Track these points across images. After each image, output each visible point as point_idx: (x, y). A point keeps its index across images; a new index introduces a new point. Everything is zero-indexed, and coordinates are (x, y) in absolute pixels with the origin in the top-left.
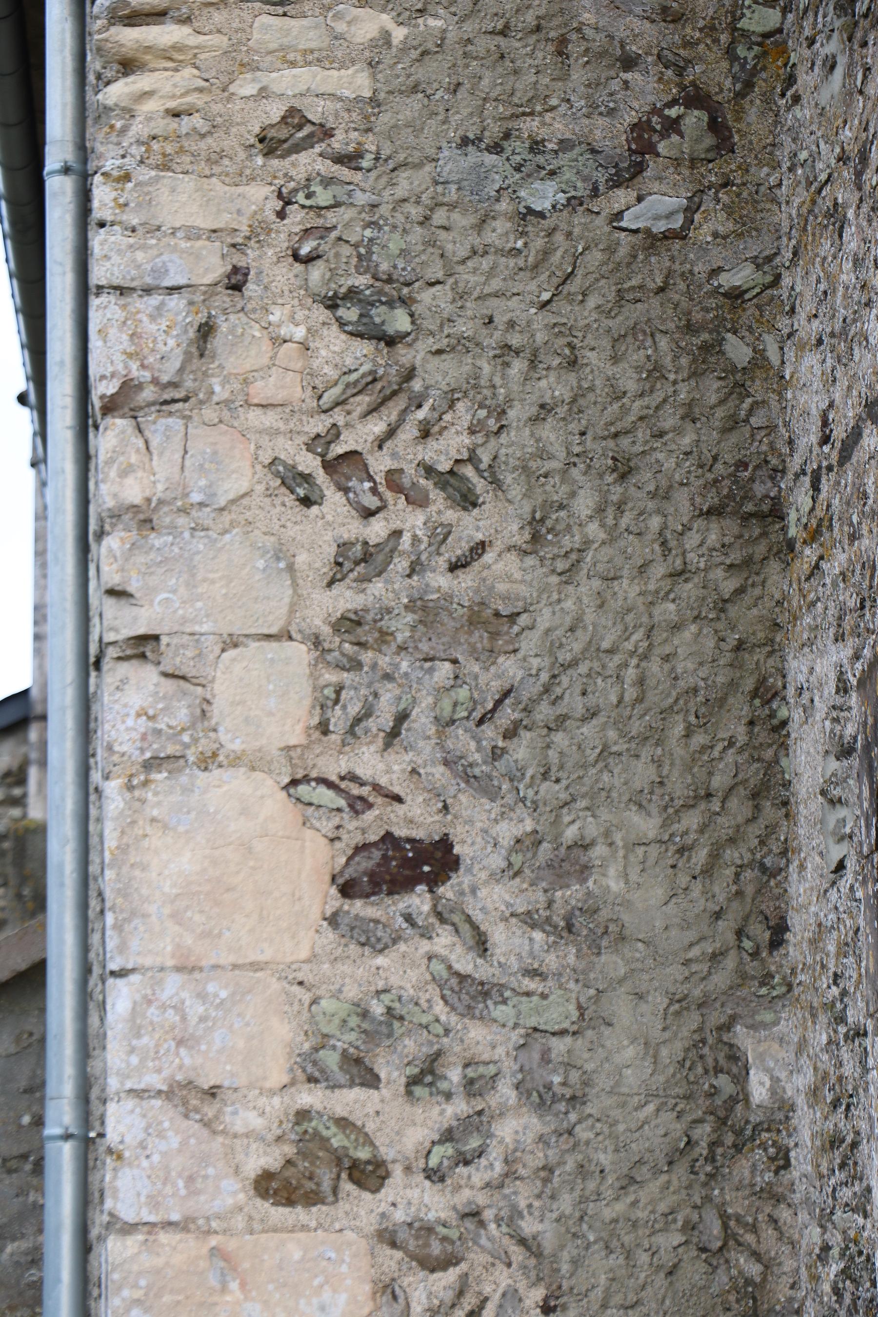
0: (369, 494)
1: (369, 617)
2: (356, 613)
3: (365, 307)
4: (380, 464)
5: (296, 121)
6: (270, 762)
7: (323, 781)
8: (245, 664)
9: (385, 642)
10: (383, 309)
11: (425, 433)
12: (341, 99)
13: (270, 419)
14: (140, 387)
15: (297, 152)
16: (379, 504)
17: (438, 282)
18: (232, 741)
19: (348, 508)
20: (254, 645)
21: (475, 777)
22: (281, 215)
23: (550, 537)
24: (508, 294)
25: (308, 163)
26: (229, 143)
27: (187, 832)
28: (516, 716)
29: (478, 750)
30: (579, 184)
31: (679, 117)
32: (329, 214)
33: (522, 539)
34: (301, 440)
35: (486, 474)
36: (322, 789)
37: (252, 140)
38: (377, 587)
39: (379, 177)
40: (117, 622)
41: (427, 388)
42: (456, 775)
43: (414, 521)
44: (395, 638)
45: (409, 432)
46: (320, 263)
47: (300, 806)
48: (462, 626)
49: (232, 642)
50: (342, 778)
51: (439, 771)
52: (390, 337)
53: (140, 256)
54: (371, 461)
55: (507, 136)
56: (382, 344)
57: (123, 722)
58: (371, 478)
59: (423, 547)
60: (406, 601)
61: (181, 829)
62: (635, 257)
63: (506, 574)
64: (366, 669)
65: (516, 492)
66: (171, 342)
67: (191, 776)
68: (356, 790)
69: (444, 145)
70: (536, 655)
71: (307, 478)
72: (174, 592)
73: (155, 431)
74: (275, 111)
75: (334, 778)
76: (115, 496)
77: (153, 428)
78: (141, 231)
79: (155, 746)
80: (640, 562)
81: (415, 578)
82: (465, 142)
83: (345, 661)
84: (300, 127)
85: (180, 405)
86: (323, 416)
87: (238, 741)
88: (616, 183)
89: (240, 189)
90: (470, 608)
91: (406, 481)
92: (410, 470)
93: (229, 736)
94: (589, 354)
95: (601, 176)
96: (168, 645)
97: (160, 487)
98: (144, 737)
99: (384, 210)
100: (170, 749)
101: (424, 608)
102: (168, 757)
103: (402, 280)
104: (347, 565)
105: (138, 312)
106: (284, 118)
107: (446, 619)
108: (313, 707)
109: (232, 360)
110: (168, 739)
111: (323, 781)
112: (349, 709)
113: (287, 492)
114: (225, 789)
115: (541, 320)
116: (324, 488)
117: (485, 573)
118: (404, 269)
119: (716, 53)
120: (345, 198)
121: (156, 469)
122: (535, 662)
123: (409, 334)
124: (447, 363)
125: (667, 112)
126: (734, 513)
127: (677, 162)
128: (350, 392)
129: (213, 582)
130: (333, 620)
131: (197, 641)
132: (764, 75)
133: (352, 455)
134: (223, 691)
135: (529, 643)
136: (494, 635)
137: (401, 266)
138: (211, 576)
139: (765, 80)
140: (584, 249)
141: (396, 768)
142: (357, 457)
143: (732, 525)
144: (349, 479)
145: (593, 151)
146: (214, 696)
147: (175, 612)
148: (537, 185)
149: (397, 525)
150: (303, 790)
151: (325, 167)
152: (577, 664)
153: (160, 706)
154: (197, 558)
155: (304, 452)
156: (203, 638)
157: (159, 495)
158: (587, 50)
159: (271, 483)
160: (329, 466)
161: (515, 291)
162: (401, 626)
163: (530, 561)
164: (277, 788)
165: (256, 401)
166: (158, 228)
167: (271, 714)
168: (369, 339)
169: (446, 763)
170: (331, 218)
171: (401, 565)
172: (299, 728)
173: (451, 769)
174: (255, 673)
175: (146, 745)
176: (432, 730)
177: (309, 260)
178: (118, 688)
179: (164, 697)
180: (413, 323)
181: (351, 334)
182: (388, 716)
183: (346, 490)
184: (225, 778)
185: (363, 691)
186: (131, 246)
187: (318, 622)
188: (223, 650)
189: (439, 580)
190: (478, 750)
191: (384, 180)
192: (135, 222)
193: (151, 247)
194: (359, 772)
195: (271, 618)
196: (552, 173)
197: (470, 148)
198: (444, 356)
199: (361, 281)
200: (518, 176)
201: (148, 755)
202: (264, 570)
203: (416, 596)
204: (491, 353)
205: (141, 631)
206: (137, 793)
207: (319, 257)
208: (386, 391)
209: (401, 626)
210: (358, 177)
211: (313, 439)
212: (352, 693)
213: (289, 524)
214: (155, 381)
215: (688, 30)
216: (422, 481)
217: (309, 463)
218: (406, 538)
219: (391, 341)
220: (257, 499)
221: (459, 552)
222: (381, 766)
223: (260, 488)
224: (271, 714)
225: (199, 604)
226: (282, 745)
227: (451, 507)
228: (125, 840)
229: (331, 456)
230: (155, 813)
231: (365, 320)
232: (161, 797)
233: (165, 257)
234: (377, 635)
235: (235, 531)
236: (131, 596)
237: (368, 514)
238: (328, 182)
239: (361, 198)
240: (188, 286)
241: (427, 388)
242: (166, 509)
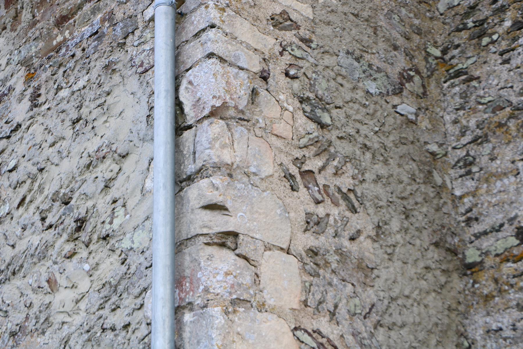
0: (318, 193)
1: (321, 252)
2: (316, 248)
3: (312, 105)
4: (321, 181)
5: (286, 17)
6: (286, 315)
7: (306, 331)
8: (274, 260)
9: (326, 266)
10: (320, 111)
11: (93, 258)
12: (302, 15)
13: (278, 143)
14: (228, 108)
15: (286, 30)
16: (322, 199)
17: (340, 108)
18: (270, 299)
19: (309, 196)
20: (277, 252)
21: (365, 345)
22: (281, 54)
23: (382, 236)
24: (363, 123)
25: (289, 36)
26: (261, 15)
27: (253, 344)
28: (378, 318)
29: (366, 331)
30: (383, 88)
31: (413, 76)
32: (300, 61)
33: (373, 233)
34: (291, 158)
35: (359, 199)
36: (306, 335)
37: (269, 18)
38: (322, 238)
39: (318, 53)
40: (211, 223)
41: (336, 152)
42: (357, 343)
43: (335, 212)
44: (331, 266)
45: (330, 170)
46: (297, 80)
47: (298, 342)
48: (355, 268)
49: (268, 248)
50: (314, 332)
51: (351, 338)
52: (323, 124)
53: (229, 47)
54: (318, 176)
55: (361, 57)
56: (319, 127)
57: (215, 277)
58: (317, 185)
59: (339, 225)
60: (334, 248)
61: (251, 342)
62: (402, 125)
63: (365, 247)
64: (321, 277)
65: (371, 211)
66: (243, 92)
67: (255, 313)
68: (320, 340)
69: (341, 50)
70: (383, 291)
71: (292, 177)
72: (245, 213)
73: (236, 131)
74: (278, 10)
75: (310, 331)
76: (219, 156)
77: (236, 129)
78: (229, 36)
79: (238, 292)
80: (415, 258)
81: (337, 239)
82: (348, 53)
83: (313, 271)
84: (286, 20)
85: (246, 123)
86: (299, 150)
87: (272, 300)
88: (395, 94)
89: (265, 36)
90: (358, 260)
91: (330, 192)
92: (332, 187)
93: (269, 296)
94: (390, 160)
95: (390, 88)
96: (243, 240)
97: (238, 159)
98: (232, 286)
99: (320, 68)
100: (245, 296)
101: (341, 254)
102: (244, 300)
103: (326, 101)
104: (312, 224)
105: (229, 72)
106: (281, 13)
107: (349, 263)
108: (302, 291)
109: (266, 109)
110: (244, 290)
111: (306, 331)
112: (316, 296)
113: (287, 181)
114: (268, 324)
115: (375, 138)
116: (299, 184)
117: (361, 245)
118: (327, 97)
119: (421, 58)
120: (305, 57)
121: (236, 150)
122: (382, 294)
123: (330, 126)
124: (344, 143)
125: (409, 72)
126: (443, 247)
127: (412, 93)
128: (311, 143)
129: (260, 214)
130: (306, 249)
131: (254, 242)
132: (437, 72)
133: (311, 172)
134: (265, 270)
135: (379, 283)
136: (366, 276)
137: (326, 95)
138: (260, 211)
139: (438, 74)
140: (387, 115)
141: (335, 332)
142: (312, 174)
143: (443, 253)
144: (309, 183)
145: (388, 77)
146: (261, 273)
147: (246, 224)
148: (369, 82)
149: (328, 211)
150: (298, 333)
151: (296, 40)
152: (397, 299)
153: (238, 272)
154: (254, 199)
155: (291, 164)
156: (257, 241)
157: (237, 163)
158: (384, 36)
159: (281, 174)
160: (301, 173)
161: (366, 122)
162: (333, 259)
163: (376, 245)
164: (289, 330)
165: (275, 132)
166: (236, 38)
167: (285, 289)
168: (314, 122)
169: (353, 335)
170: (301, 63)
171: (330, 231)
172: (297, 300)
173: (355, 338)
174: (278, 266)
175: (233, 291)
176: (347, 317)
177: (294, 78)
178: (208, 259)
179: (240, 268)
180: (332, 121)
181: (308, 117)
182: (331, 304)
183: (308, 188)
184: (269, 318)
185: (322, 289)
186: (226, 41)
187: (300, 248)
188: (265, 251)
189: (346, 243)
190: (366, 331)
191: (320, 55)
192: (228, 31)
193: (234, 45)
194: (322, 330)
195: (283, 240)
196: (375, 79)
197: (350, 56)
198: (342, 141)
199: (312, 96)
200: (364, 75)
201: (234, 297)
202: (280, 215)
203: (339, 248)
204: (360, 146)
205: (231, 229)
206: (230, 316)
207: (297, 78)
208: (323, 149)
209: (333, 259)
210: (309, 50)
211: (295, 160)
212: (317, 288)
213: (287, 197)
214: (236, 107)
215: (412, 45)
216: (336, 194)
217: (294, 170)
218: (331, 218)
219: (322, 126)
220: (275, 180)
221: (352, 232)
222: (329, 329)
223: (276, 175)
224: (285, 289)
225: (255, 223)
226: (290, 307)
227: (347, 210)
228: (225, 342)
229: (302, 170)
230: (239, 329)
231: (313, 113)
232: (241, 322)
233: (239, 52)
234: (324, 262)
235: (268, 192)
236: (226, 209)
237: (318, 202)
238: (299, 47)
239: (312, 60)
240: (247, 70)
241: (336, 152)
242: (239, 171)
